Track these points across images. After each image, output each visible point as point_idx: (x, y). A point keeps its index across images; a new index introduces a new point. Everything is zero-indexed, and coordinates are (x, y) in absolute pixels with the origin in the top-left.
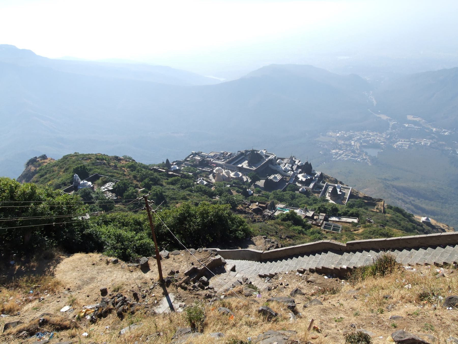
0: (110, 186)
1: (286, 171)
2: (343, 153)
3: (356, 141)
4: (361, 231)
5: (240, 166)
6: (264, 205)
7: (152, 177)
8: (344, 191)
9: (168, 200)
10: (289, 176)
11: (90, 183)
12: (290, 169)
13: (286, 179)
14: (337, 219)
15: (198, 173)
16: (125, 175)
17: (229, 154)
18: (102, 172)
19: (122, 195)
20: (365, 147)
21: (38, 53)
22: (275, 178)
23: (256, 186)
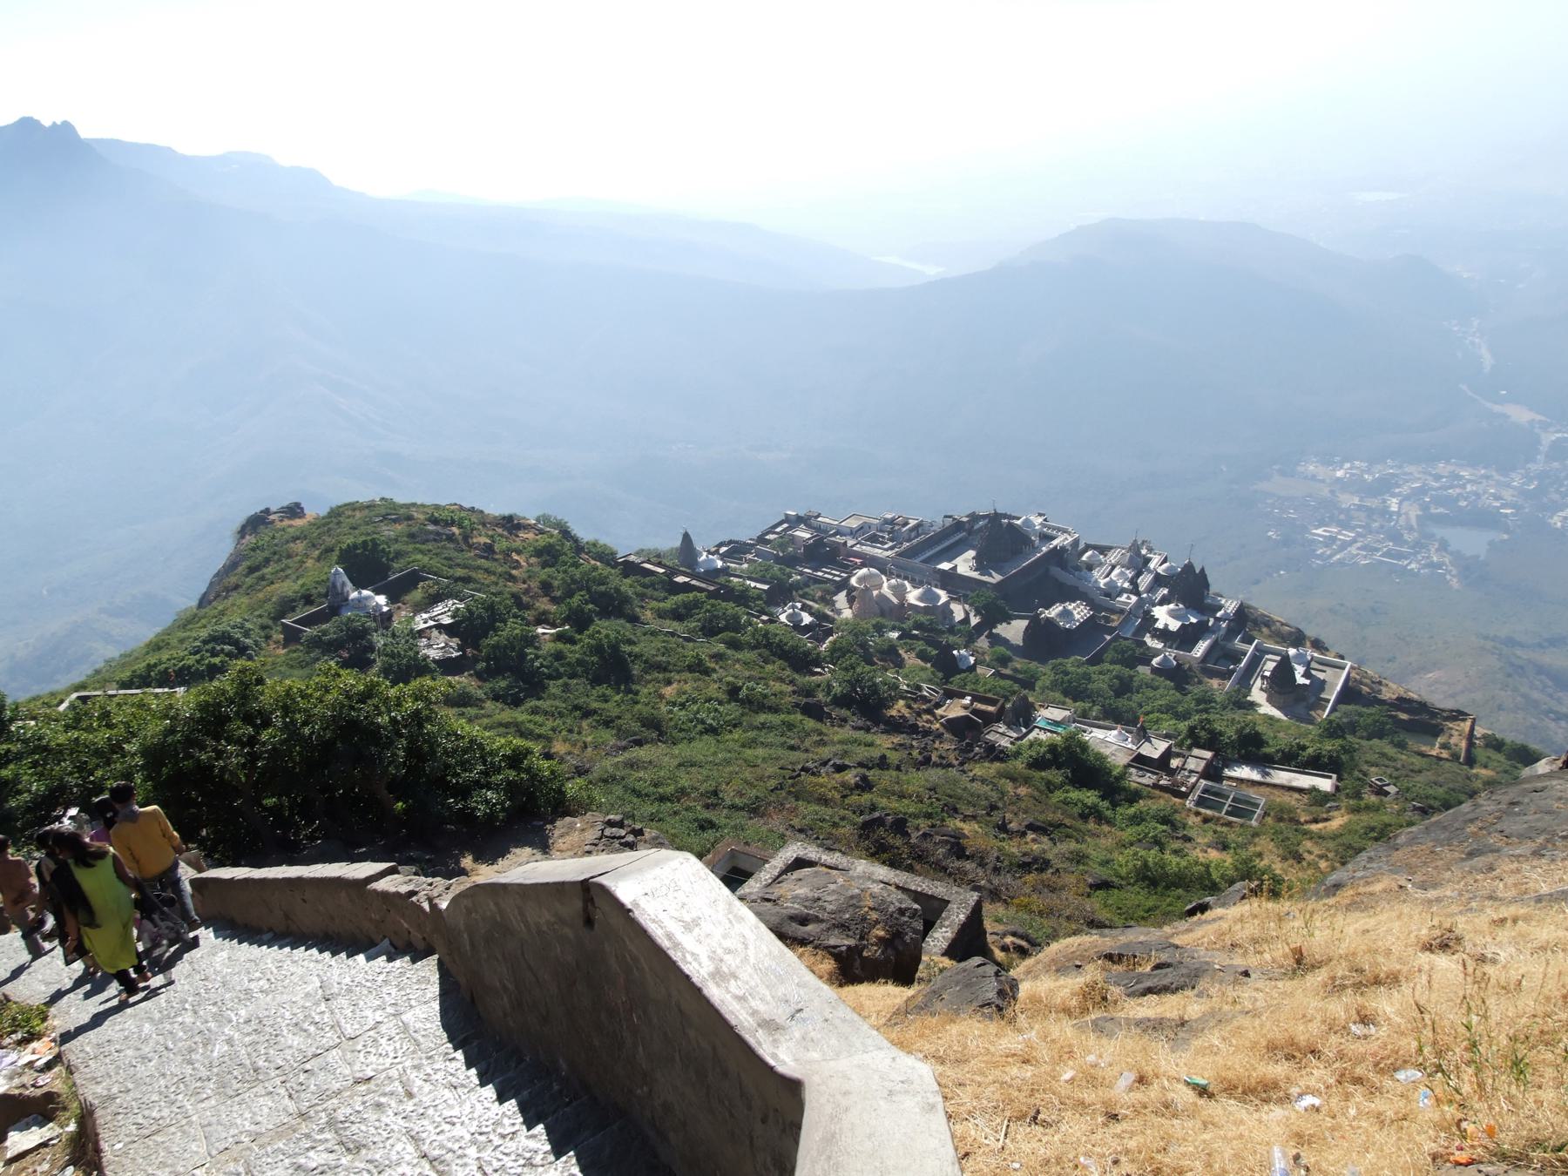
0: (444, 612)
1: (1112, 592)
2: (1354, 541)
3: (1407, 498)
4: (1338, 822)
5: (945, 566)
6: (991, 709)
7: (603, 588)
8: (1321, 676)
9: (636, 670)
10: (1122, 611)
11: (381, 600)
12: (1126, 585)
13: (1107, 620)
14: (1255, 775)
15: (796, 586)
16: (512, 578)
17: (912, 523)
18: (435, 563)
19: (476, 647)
20: (1440, 520)
21: (187, 146)
22: (1066, 614)
23: (996, 640)
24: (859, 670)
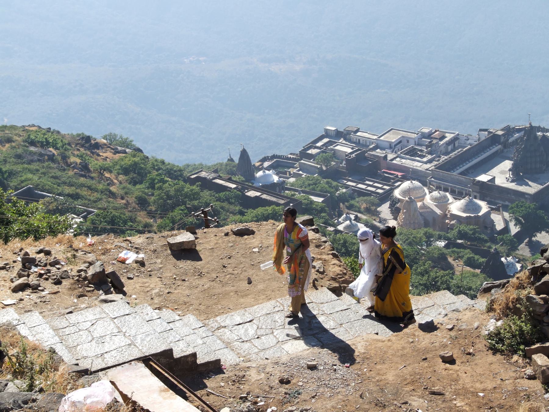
5: (483, 178)
15: (343, 199)
17: (449, 137)
18: (47, 182)
24: (432, 274)
